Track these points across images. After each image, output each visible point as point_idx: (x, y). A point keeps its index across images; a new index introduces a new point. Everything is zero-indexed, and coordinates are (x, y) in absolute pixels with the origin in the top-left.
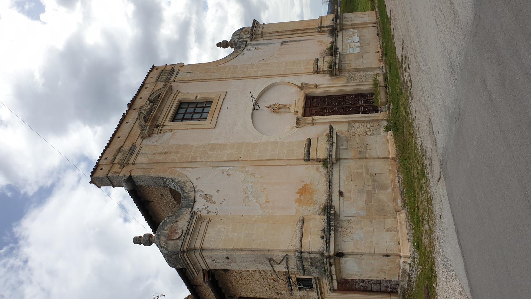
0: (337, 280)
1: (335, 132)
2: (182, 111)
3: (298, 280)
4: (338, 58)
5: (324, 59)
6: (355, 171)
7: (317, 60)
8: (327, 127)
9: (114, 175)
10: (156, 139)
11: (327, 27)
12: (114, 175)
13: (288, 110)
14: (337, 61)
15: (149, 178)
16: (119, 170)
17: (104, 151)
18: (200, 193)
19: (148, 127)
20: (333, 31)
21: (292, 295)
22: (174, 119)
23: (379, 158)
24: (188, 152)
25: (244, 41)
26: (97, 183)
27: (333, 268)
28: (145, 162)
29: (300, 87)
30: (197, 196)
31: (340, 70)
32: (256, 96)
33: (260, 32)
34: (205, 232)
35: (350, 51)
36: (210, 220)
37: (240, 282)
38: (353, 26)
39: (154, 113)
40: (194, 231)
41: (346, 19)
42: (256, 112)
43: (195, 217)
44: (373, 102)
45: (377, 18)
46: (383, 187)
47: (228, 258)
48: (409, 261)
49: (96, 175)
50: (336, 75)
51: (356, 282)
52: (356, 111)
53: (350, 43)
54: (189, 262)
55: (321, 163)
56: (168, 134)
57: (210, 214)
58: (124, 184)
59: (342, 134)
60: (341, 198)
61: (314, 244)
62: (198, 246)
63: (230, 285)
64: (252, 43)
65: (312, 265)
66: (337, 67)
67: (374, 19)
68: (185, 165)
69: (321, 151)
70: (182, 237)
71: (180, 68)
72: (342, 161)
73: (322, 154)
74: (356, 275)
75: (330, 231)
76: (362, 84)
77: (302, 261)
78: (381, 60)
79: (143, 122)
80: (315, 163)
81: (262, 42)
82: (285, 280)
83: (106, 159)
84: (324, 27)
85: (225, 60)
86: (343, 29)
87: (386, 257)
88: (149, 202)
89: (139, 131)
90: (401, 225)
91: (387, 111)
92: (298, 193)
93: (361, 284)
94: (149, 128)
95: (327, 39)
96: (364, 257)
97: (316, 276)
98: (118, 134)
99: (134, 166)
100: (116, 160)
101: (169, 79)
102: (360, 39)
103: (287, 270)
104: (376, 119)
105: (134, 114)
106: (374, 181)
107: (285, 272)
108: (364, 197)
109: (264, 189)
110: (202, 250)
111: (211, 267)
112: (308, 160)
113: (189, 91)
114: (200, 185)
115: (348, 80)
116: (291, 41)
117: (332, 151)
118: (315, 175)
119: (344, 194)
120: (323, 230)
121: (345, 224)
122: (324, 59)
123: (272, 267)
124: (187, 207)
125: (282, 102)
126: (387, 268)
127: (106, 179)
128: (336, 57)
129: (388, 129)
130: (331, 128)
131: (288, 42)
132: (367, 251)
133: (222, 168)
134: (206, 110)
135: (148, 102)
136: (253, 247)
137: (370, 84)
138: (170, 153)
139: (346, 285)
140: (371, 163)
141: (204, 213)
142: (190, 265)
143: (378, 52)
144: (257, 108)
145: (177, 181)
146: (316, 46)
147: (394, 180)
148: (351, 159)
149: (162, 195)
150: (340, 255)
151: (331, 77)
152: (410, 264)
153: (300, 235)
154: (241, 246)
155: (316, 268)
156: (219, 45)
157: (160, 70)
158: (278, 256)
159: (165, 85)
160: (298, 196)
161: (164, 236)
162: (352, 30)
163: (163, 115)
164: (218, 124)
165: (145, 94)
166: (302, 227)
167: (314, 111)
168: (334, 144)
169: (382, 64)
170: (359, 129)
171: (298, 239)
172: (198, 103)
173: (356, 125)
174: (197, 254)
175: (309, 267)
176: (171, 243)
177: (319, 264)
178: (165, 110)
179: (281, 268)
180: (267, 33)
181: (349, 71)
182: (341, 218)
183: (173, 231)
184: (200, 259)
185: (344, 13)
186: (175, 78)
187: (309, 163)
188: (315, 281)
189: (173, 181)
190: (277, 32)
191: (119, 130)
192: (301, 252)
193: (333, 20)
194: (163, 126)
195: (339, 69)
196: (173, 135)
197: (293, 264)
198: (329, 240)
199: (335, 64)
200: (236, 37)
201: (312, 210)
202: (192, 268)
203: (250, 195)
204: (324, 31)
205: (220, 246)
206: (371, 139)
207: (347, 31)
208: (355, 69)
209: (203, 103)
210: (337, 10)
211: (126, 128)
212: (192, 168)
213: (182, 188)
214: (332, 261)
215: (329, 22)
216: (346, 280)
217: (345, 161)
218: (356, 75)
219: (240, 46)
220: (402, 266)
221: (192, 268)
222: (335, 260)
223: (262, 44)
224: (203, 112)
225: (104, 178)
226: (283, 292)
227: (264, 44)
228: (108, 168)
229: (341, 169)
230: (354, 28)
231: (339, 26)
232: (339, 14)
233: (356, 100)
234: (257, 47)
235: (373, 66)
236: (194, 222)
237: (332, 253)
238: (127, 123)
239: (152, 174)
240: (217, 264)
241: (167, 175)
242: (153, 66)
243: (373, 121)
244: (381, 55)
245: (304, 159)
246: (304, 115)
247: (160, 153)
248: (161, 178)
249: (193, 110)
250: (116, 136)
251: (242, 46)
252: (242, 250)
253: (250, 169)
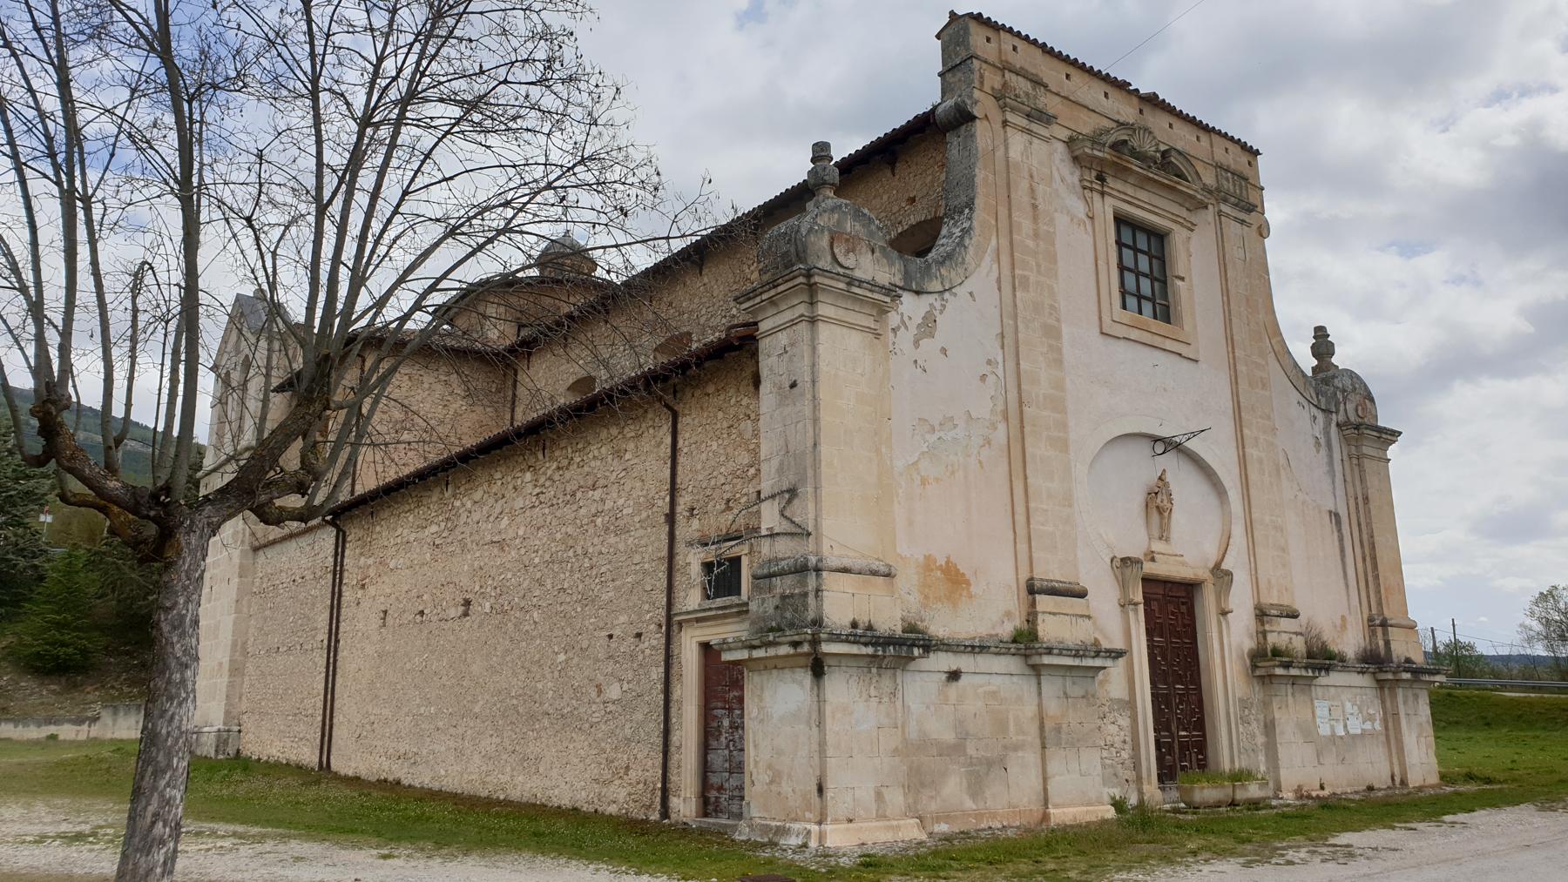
0: (750, 659)
1: (1108, 663)
2: (1142, 242)
3: (736, 562)
4: (1304, 673)
5: (1297, 634)
7: (1294, 615)
8: (1119, 644)
9: (977, 75)
10: (1069, 179)
11: (1387, 643)
12: (977, 75)
13: (1156, 533)
14: (1293, 672)
15: (971, 167)
16: (987, 88)
18: (938, 305)
20: (1375, 662)
21: (690, 544)
22: (1121, 220)
23: (1045, 780)
24: (1038, 265)
25: (1337, 404)
26: (950, 31)
27: (784, 650)
28: (1012, 154)
29: (1217, 566)
30: (931, 299)
31: (1267, 680)
32: (1192, 445)
33: (1365, 450)
34: (851, 326)
35: (1321, 709)
36: (877, 336)
37: (720, 415)
38: (1391, 721)
39: (1135, 165)
40: (856, 299)
41: (1411, 699)
42: (1145, 448)
43: (888, 299)
44: (1183, 768)
45: (1420, 789)
46: (976, 787)
47: (793, 385)
48: (813, 844)
49: (973, 27)
50: (1254, 667)
51: (731, 710)
52: (1161, 724)
53: (1343, 707)
54: (781, 288)
55: (1026, 626)
56: (1080, 209)
57: (891, 335)
58: (950, 103)
59: (1101, 683)
60: (944, 676)
61: (840, 604)
62: (823, 310)
63: (711, 389)
64: (1333, 428)
65: (783, 597)
66: (1279, 671)
67: (1414, 780)
68: (1005, 259)
69: (1055, 626)
70: (841, 271)
71: (1254, 228)
72: (1033, 680)
73: (1050, 629)
74: (761, 709)
75: (874, 645)
76: (1232, 738)
77: (796, 572)
78: (1299, 793)
79: (1112, 139)
80: (1025, 609)
81: (1337, 456)
82: (734, 527)
83: (1015, 48)
84: (1385, 633)
85: (1282, 353)
86: (1382, 688)
87: (815, 788)
88: (892, 165)
89: (1086, 130)
90: (892, 827)
91: (1167, 806)
92: (947, 563)
93: (726, 723)
95: (1350, 643)
96: (815, 729)
97: (753, 606)
98: (1077, 76)
99: (998, 126)
100: (1014, 77)
101: (1225, 201)
102: (1355, 736)
103: (764, 532)
104: (1144, 774)
105: (1127, 111)
106: (990, 764)
107: (757, 529)
108: (949, 737)
109: (953, 473)
110: (813, 321)
111: (764, 345)
112: (1032, 590)
113: (1195, 256)
114: (957, 303)
115: (1241, 700)
116: (1341, 540)
117: (1060, 654)
118: (991, 610)
119: (954, 684)
120: (870, 628)
121: (886, 682)
122: (1297, 634)
123: (773, 497)
124: (907, 275)
125: (1179, 519)
126: (786, 788)
127: (964, 54)
128: (1306, 668)
129: (1118, 805)
130: (1116, 654)
131: (1340, 530)
132: (830, 738)
133: (1000, 359)
134: (1147, 307)
135: (1163, 148)
136: (824, 449)
137: (1232, 761)
138: (1035, 219)
139: (723, 684)
140: (1031, 757)
141: (893, 319)
142: (772, 292)
143: (1322, 788)
144: (1160, 448)
145: (967, 242)
146: (1329, 610)
147: (994, 816)
148: (1040, 705)
149: (912, 200)
150: (818, 669)
152: (805, 845)
153: (857, 567)
154: (826, 418)
155: (777, 607)
156: (1321, 333)
157: (1247, 171)
158: (803, 512)
159: (1210, 192)
160: (942, 561)
161: (838, 221)
162: (1379, 717)
163: (1130, 191)
164: (1112, 341)
165: (1183, 138)
166: (874, 573)
167: (1155, 606)
168: (1077, 662)
169: (1288, 796)
170: (1116, 729)
171: (846, 562)
172: (1164, 283)
173: (1124, 722)
174: (802, 309)
175: (778, 590)
176: (825, 242)
177: (788, 615)
178: (1143, 195)
179: (770, 517)
180: (1362, 471)
181: (1266, 705)
182: (899, 672)
183: (852, 245)
184: (788, 316)
185: (1431, 694)
186: (1228, 216)
187: (1024, 592)
188: (738, 605)
189: (966, 232)
190: (1366, 499)
191: (1086, 76)
192: (818, 570)
193: (1408, 660)
194: (1103, 194)
195: (1271, 676)
196: (1081, 223)
197: (785, 549)
198: (854, 643)
199: (1287, 666)
200: (1347, 382)
201: (911, 598)
202: (765, 296)
203: (935, 437)
204: (1373, 633)
205: (823, 366)
206: (1092, 760)
207: (1377, 702)
208: (1273, 722)
209: (1165, 295)
210: (1438, 672)
211: (1092, 93)
212: (999, 281)
213: (949, 256)
214: (806, 648)
215: (1401, 648)
216: (738, 684)
217: (1034, 688)
218: (1254, 724)
219: (1324, 394)
220: (796, 826)
221: (765, 296)
222: (807, 655)
223: (1330, 456)
224: (1140, 297)
225: (967, 49)
226: (695, 523)
227: (1331, 463)
228: (992, 58)
229: (1015, 679)
230: (1385, 721)
231: (1390, 676)
232: (1427, 678)
233: (1189, 722)
234: (1322, 441)
235: (1283, 772)
236: (876, 296)
237: (827, 648)
238: (1106, 95)
239: (980, 175)
240: (774, 359)
241: (981, 215)
242: (1257, 153)
243: (1136, 766)
244: (1314, 794)
245: (1032, 579)
246: (1148, 581)
248: (972, 199)
249: (1145, 271)
250: (1173, 120)
251: (1323, 400)
252: (816, 421)
253: (1000, 435)
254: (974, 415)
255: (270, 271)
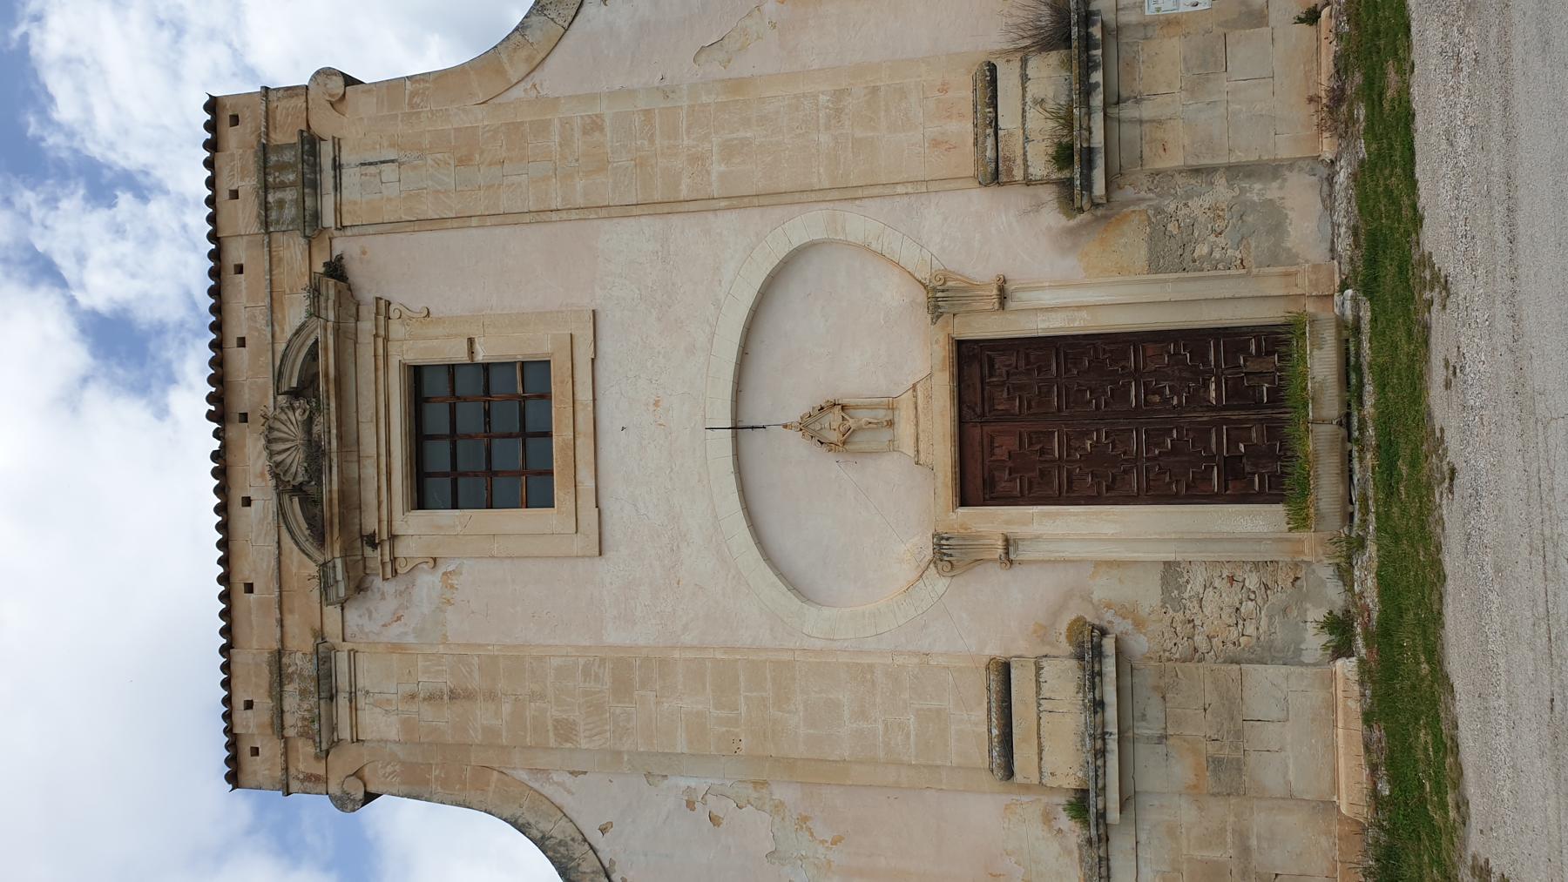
6: (1197, 854)
13: (886, 435)
17: (226, 668)
19: (339, 563)
83: (249, 705)
94: (345, 565)
98: (243, 572)
115: (1154, 266)
138: (469, 696)
151: (1070, 216)
191: (236, 546)
229: (1143, 837)
235: (1285, 152)
242: (212, 105)
247: (430, 698)
254: (769, 846)
255: (284, 529)
